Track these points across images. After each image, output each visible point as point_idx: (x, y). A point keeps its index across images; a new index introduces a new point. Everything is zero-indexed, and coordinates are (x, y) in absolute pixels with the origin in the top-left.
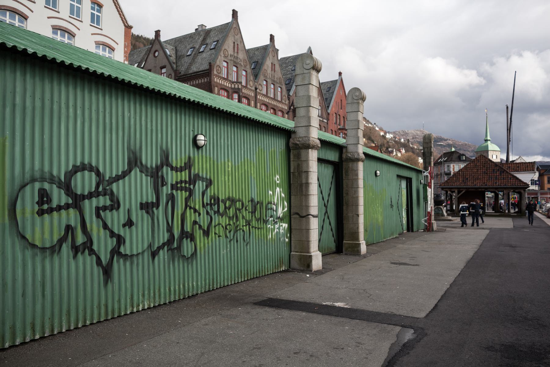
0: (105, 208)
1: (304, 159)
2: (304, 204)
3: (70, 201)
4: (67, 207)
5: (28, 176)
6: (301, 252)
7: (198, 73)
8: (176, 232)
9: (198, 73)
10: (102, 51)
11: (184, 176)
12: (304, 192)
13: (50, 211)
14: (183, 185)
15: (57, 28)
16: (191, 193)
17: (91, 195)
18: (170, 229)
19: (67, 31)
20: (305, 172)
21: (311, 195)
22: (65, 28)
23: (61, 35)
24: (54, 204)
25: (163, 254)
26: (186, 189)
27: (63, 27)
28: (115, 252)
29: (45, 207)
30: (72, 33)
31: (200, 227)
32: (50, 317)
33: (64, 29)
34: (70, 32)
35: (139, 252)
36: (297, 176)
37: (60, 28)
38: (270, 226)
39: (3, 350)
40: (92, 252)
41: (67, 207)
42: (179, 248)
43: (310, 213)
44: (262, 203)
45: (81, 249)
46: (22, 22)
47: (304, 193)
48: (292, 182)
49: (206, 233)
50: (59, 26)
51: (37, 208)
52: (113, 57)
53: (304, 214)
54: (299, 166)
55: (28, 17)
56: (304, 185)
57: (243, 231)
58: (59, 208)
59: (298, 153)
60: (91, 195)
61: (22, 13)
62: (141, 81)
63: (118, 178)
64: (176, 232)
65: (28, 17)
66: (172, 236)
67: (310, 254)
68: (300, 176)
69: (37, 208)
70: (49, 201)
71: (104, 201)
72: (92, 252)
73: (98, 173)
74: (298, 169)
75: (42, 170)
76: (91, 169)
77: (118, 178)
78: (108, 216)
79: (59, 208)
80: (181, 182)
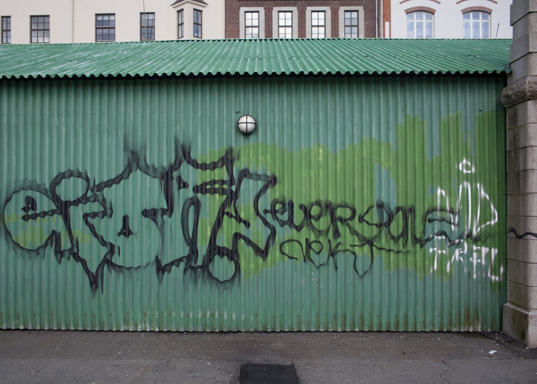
0: (94, 215)
1: (522, 124)
2: (521, 213)
3: (54, 208)
4: (53, 212)
5: (13, 186)
6: (518, 306)
7: (377, 22)
8: (203, 248)
9: (377, 22)
10: (482, 19)
11: (222, 174)
12: (522, 188)
13: (34, 217)
14: (217, 186)
15: (468, 10)
16: (233, 197)
17: (76, 202)
18: (192, 243)
19: (481, 9)
20: (522, 148)
21: (532, 193)
22: (478, 7)
23: (473, 17)
24: (38, 211)
25: (178, 271)
26: (222, 192)
27: (476, 7)
28: (107, 262)
29: (30, 212)
30: (487, 10)
31: (249, 242)
32: (378, 314)
33: (477, 9)
34: (485, 10)
35: (321, 263)
36: (513, 157)
37: (472, 10)
38: (435, 249)
39: (1, 329)
40: (77, 257)
41: (53, 212)
42: (205, 267)
43: (529, 229)
44: (412, 210)
45: (66, 254)
46: (430, 19)
47: (521, 192)
48: (507, 172)
49: (263, 253)
50: (471, 8)
51: (22, 213)
52: (489, 22)
53: (521, 233)
54: (516, 138)
55: (435, 11)
56: (522, 174)
57: (354, 253)
58: (44, 214)
59: (514, 113)
60: (76, 202)
61: (429, 8)
62: (43, 73)
63: (109, 183)
64: (203, 248)
65: (435, 11)
66: (194, 252)
67: (527, 313)
68: (517, 158)
69: (22, 213)
70: (34, 208)
71: (96, 207)
72: (77, 257)
73: (87, 179)
74: (514, 143)
75: (25, 180)
76: (79, 175)
77: (109, 183)
78: (98, 223)
79: (44, 214)
80: (214, 182)
